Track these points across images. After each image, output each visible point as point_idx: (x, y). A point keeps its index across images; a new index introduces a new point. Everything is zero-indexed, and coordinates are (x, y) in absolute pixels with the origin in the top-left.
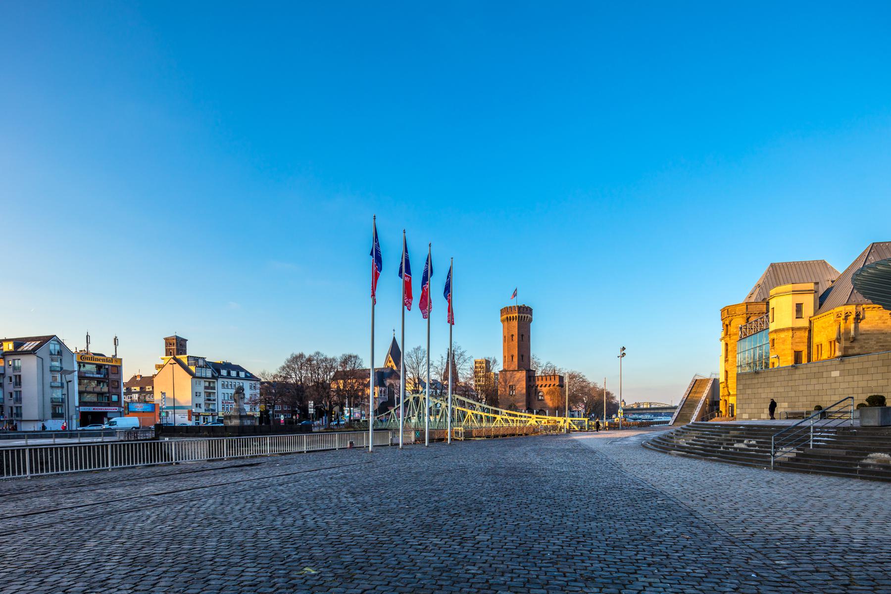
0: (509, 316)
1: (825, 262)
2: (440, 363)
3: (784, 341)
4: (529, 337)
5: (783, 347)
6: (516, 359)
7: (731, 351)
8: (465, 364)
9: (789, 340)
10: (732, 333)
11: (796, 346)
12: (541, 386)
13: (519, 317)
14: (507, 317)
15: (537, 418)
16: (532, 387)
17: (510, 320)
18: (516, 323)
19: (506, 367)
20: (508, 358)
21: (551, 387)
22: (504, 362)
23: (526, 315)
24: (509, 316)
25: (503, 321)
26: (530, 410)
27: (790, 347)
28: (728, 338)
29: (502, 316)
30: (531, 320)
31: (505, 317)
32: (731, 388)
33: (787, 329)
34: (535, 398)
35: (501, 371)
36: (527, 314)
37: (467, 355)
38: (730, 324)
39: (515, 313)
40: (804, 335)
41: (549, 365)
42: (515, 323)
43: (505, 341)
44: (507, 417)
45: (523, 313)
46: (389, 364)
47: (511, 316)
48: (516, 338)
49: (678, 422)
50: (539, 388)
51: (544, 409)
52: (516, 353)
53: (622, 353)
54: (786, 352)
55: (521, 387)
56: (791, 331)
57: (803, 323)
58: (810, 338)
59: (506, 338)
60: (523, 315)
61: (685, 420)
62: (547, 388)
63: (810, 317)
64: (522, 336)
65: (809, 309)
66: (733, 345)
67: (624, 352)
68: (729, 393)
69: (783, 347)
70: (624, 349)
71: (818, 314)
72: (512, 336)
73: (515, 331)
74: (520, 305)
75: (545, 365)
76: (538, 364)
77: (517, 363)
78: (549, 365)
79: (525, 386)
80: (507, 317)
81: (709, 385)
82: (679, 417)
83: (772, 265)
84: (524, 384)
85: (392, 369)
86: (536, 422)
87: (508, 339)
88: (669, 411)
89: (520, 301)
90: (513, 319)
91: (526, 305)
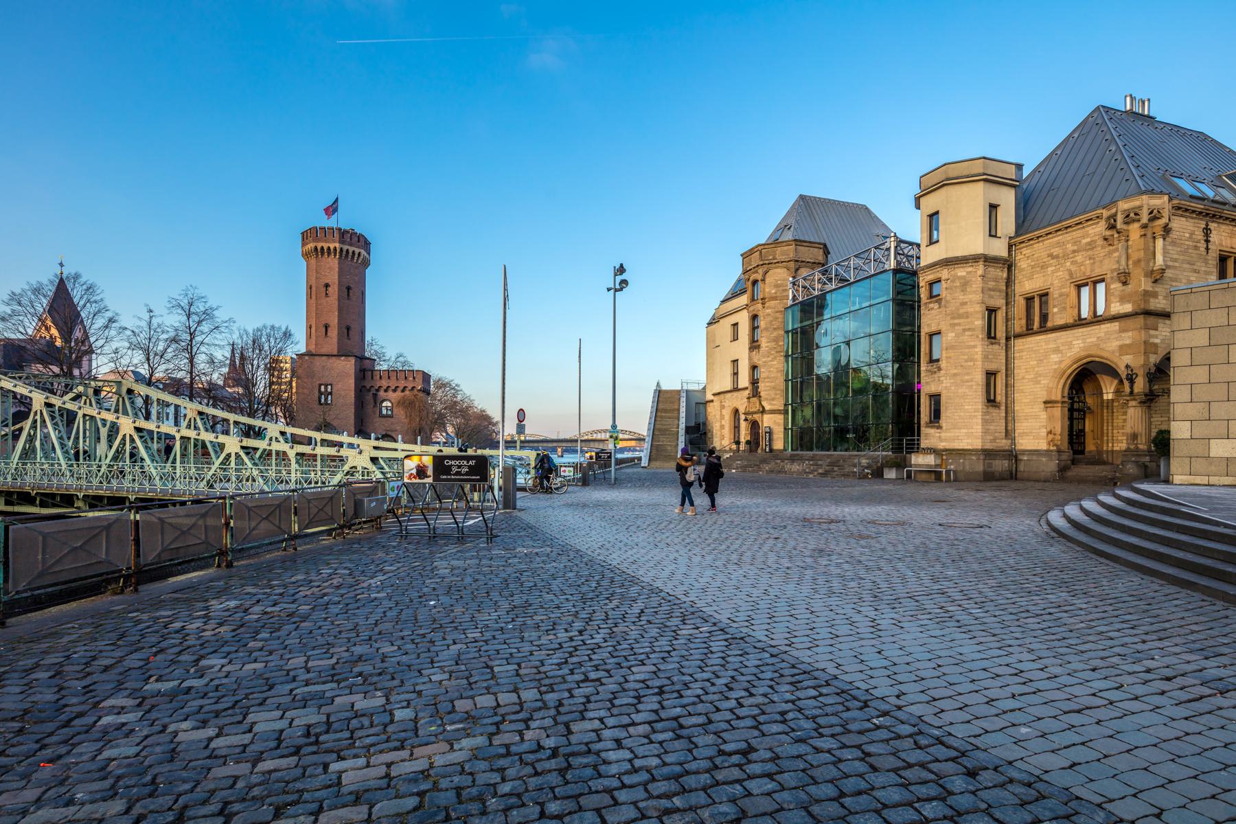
0: (319, 245)
1: (867, 208)
2: (144, 324)
3: (965, 284)
4: (363, 294)
5: (962, 297)
6: (334, 333)
7: (766, 329)
8: (218, 336)
9: (977, 284)
10: (767, 296)
11: (991, 297)
12: (386, 391)
13: (341, 250)
14: (316, 248)
15: (375, 448)
16: (369, 390)
17: (323, 254)
18: (336, 261)
19: (313, 348)
20: (318, 328)
21: (407, 392)
22: (309, 336)
23: (357, 251)
24: (319, 245)
25: (306, 255)
26: (362, 432)
27: (978, 297)
28: (760, 306)
29: (303, 245)
30: (366, 263)
31: (311, 246)
32: (767, 399)
33: (975, 259)
34: (374, 413)
35: (302, 355)
36: (358, 247)
37: (221, 316)
38: (763, 280)
39: (334, 241)
40: (1000, 274)
41: (401, 359)
42: (333, 263)
43: (309, 296)
44: (283, 446)
45: (351, 245)
46: (44, 333)
47: (325, 246)
48: (334, 290)
49: (656, 460)
50: (382, 393)
51: (393, 435)
52: (334, 321)
53: (619, 278)
54: (970, 310)
55: (346, 387)
56: (981, 264)
57: (999, 248)
58: (1009, 282)
59: (314, 289)
60: (351, 249)
61: (665, 456)
62: (399, 394)
63: (1010, 238)
64: (349, 288)
65: (1007, 222)
66: (770, 319)
67: (624, 277)
68: (763, 407)
69: (962, 297)
70: (621, 270)
71: (1021, 235)
72: (327, 286)
73: (333, 278)
74: (344, 227)
75: (393, 359)
76: (381, 356)
77: (335, 340)
78: (401, 359)
79: (353, 386)
80: (316, 248)
81: (683, 400)
82: (654, 451)
83: (802, 197)
84: (351, 382)
85: (51, 342)
86: (374, 460)
87: (316, 292)
88: (550, 445)
89: (342, 220)
90: (329, 253)
91: (358, 231)
